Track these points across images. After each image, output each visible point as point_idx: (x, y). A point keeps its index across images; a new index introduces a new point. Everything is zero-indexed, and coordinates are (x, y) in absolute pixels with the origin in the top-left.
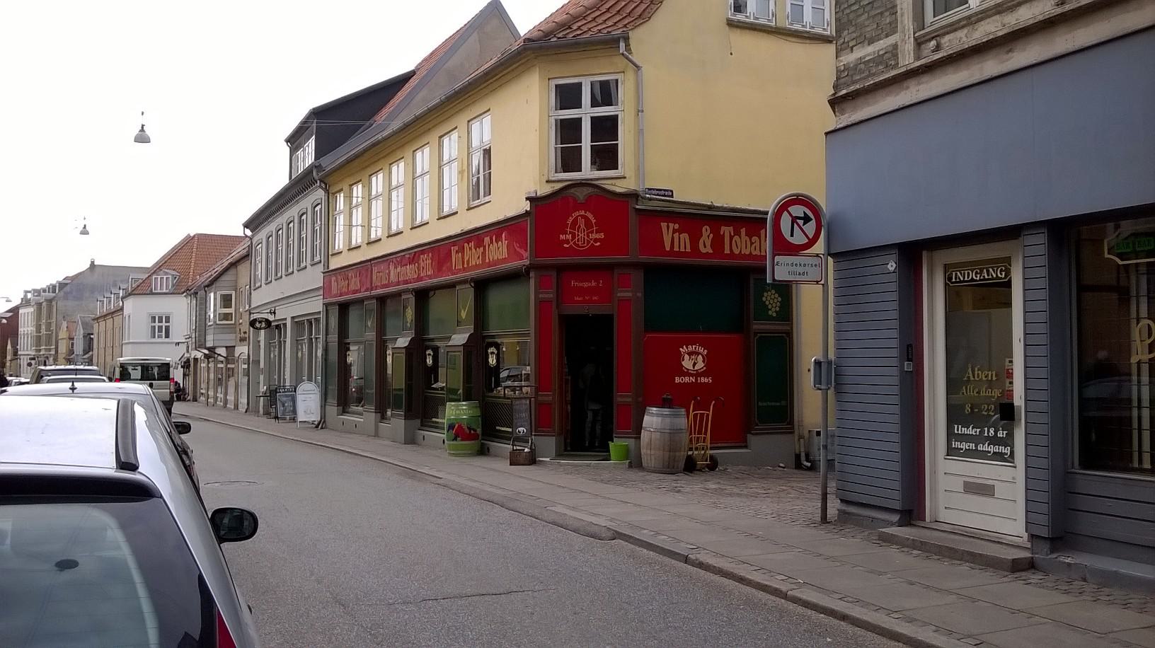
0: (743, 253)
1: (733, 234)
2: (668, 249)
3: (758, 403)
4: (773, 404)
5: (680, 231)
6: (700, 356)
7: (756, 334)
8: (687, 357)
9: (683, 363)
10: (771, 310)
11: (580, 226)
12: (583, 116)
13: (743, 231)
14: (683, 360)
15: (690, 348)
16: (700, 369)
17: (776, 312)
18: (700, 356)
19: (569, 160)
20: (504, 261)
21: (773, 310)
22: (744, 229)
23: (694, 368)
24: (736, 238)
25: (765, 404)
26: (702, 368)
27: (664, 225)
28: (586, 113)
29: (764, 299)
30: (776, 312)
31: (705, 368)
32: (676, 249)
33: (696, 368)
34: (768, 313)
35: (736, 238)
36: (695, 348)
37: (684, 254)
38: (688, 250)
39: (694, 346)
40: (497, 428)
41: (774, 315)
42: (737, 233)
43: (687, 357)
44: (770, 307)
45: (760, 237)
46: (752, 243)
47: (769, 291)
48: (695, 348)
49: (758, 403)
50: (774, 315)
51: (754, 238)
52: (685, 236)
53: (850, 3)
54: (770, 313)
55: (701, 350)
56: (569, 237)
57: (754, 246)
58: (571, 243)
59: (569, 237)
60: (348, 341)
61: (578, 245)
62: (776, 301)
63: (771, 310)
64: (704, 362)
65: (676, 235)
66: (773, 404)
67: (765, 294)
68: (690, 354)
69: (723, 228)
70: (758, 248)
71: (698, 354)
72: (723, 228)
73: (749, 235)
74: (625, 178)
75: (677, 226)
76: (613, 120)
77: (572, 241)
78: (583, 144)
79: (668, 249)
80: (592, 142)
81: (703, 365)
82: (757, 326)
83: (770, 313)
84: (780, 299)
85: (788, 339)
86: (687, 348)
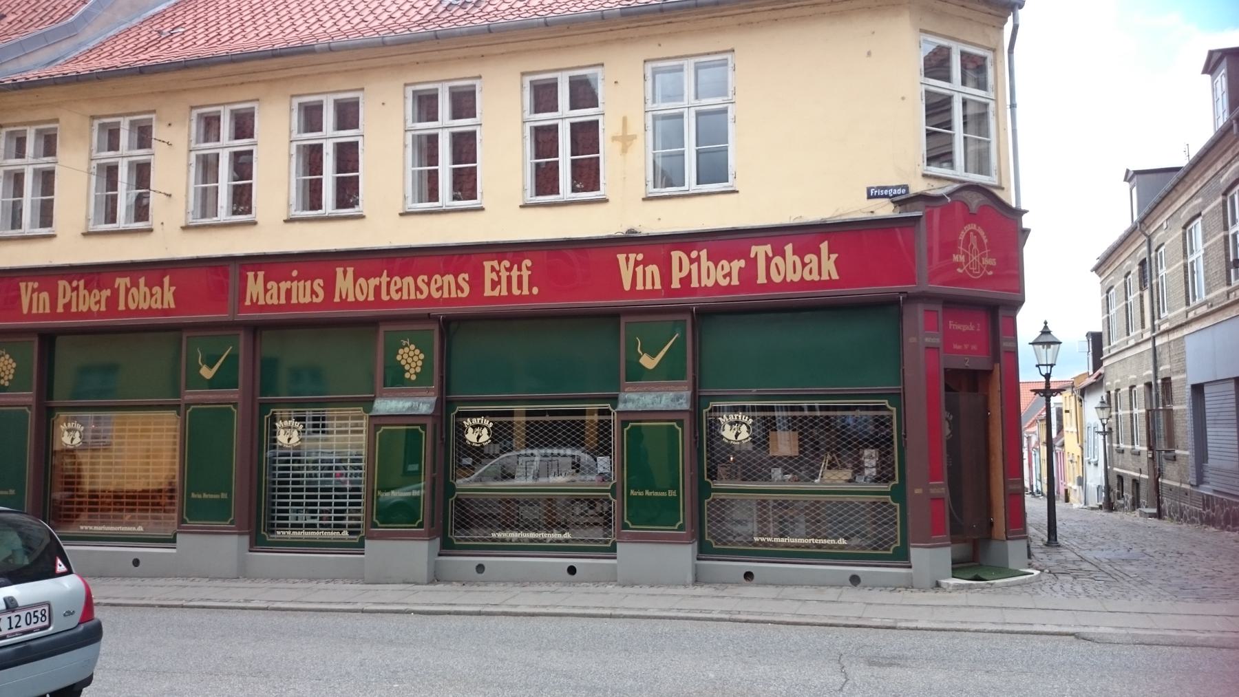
0: (140, 308)
4: (211, 496)
6: (485, 429)
8: (470, 430)
9: (723, 433)
10: (408, 371)
11: (972, 246)
12: (560, 123)
13: (142, 281)
14: (467, 433)
15: (70, 426)
17: (416, 373)
18: (485, 429)
19: (939, 154)
20: (100, 314)
21: (412, 371)
22: (263, 273)
24: (134, 290)
27: (621, 258)
28: (564, 117)
29: (399, 358)
30: (9, 380)
32: (640, 287)
33: (480, 441)
34: (404, 375)
35: (134, 290)
37: (653, 293)
41: (414, 378)
42: (135, 284)
43: (470, 430)
44: (407, 367)
45: (162, 287)
46: (152, 295)
47: (407, 346)
50: (414, 378)
51: (807, 259)
52: (653, 269)
53: (74, 2)
54: (407, 375)
55: (78, 427)
56: (962, 258)
57: (154, 298)
58: (965, 268)
59: (962, 258)
60: (56, 402)
61: (971, 271)
62: (9, 367)
63: (416, 373)
64: (489, 434)
65: (640, 269)
66: (211, 496)
67: (401, 351)
68: (474, 427)
69: (754, 249)
70: (275, 296)
71: (75, 430)
72: (754, 249)
73: (149, 285)
74: (737, 192)
76: (593, 126)
77: (966, 263)
78: (686, 149)
79: (627, 287)
80: (454, 164)
81: (488, 437)
83: (407, 375)
86: (728, 417)
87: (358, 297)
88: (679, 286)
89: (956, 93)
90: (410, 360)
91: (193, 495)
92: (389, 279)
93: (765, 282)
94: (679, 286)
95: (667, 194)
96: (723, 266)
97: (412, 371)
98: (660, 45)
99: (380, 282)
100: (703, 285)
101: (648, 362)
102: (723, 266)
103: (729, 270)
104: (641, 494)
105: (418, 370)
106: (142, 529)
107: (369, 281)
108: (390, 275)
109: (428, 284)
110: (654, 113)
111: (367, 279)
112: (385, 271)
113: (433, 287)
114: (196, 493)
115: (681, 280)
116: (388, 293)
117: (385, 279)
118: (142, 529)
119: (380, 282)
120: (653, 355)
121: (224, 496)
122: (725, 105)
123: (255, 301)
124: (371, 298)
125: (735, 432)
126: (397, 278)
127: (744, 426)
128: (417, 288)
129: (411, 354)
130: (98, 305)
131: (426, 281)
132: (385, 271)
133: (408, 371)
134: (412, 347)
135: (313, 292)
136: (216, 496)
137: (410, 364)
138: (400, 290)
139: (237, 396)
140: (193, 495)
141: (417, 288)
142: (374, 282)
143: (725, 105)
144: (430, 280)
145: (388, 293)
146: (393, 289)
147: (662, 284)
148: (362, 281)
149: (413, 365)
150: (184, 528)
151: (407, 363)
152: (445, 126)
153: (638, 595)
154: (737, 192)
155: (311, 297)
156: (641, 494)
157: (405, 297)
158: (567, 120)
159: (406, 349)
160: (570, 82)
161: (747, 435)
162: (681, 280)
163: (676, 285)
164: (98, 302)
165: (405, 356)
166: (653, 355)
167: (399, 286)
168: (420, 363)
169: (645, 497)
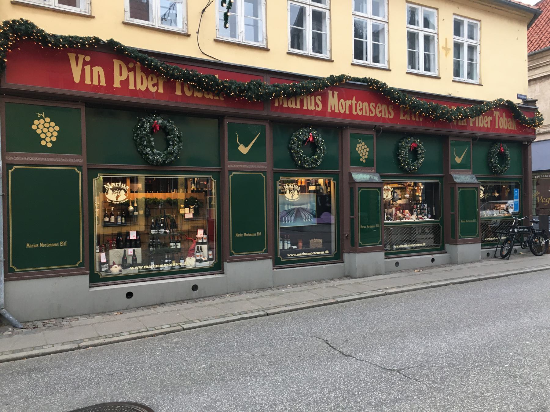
1: (499, 116)
2: (77, 79)
3: (460, 221)
5: (93, 64)
7: (230, 172)
10: (362, 157)
16: (296, 199)
17: (51, 142)
18: (296, 191)
21: (48, 139)
23: (117, 200)
25: (464, 222)
26: (297, 198)
30: (51, 142)
31: (299, 198)
32: (88, 81)
33: (293, 198)
35: (501, 119)
36: (118, 185)
37: (99, 87)
38: (103, 83)
39: (117, 184)
40: (434, 215)
44: (361, 155)
47: (42, 118)
48: (118, 185)
49: (460, 221)
50: (50, 145)
52: (98, 70)
67: (358, 146)
68: (113, 189)
75: (88, 59)
76: (425, 50)
82: (231, 165)
83: (43, 143)
84: (57, 128)
85: (265, 177)
87: (289, 105)
88: (120, 86)
89: (307, 6)
90: (45, 130)
91: (237, 235)
92: (356, 102)
93: (330, 111)
94: (120, 86)
95: (458, 80)
96: (379, 107)
97: (48, 139)
98: (458, 8)
99: (352, 103)
100: (138, 89)
101: (243, 150)
102: (379, 107)
103: (362, 107)
104: (241, 235)
105: (54, 139)
106: (328, 252)
107: (346, 102)
108: (357, 100)
109: (375, 108)
110: (455, 40)
111: (345, 100)
112: (354, 98)
113: (378, 110)
114: (239, 234)
115: (121, 82)
116: (356, 111)
117: (354, 102)
118: (328, 252)
119: (352, 103)
120: (246, 146)
121: (259, 234)
122: (477, 45)
123: (333, 109)
124: (347, 112)
125: (116, 195)
126: (360, 102)
127: (123, 191)
128: (370, 110)
129: (47, 125)
130: (156, 87)
131: (374, 106)
132: (354, 98)
133: (44, 139)
134: (48, 119)
135: (316, 104)
136: (254, 235)
137: (45, 134)
138: (361, 110)
139: (82, 161)
140: (237, 235)
141: (370, 110)
142: (349, 102)
143: (477, 45)
144: (376, 106)
145: (356, 111)
146: (358, 108)
147: (106, 82)
148: (342, 101)
149: (49, 134)
150: (11, 276)
151: (43, 132)
152: (464, 39)
153: (171, 311)
154: (482, 85)
155: (315, 107)
156: (241, 235)
157: (364, 114)
158: (423, 32)
159: (42, 121)
160: (454, 21)
161: (125, 197)
162: (121, 82)
163: (117, 85)
164: (487, 123)
165: (41, 127)
166: (246, 146)
167: (361, 107)
168: (55, 134)
169: (40, 248)
